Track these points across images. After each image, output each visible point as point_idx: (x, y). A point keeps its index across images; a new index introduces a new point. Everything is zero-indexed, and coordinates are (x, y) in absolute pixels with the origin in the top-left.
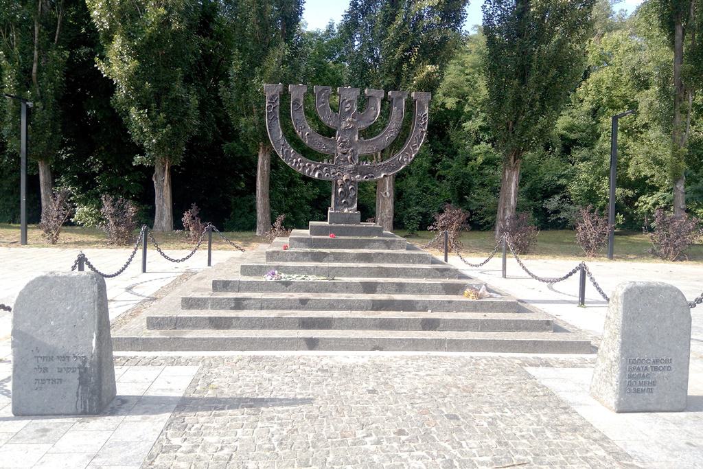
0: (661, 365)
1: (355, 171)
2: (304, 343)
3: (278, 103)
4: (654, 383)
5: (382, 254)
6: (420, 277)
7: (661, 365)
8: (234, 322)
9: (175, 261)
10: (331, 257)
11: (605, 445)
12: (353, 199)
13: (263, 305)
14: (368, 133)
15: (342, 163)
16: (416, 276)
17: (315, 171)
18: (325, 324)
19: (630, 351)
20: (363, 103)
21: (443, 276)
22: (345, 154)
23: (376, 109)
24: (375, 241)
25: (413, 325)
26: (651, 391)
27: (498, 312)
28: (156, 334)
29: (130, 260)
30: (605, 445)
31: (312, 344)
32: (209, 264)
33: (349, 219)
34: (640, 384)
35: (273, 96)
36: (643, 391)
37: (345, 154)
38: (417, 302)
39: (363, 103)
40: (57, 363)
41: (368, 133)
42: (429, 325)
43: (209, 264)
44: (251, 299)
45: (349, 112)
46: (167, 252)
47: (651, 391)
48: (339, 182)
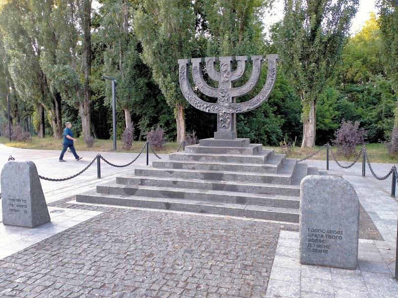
0: (334, 235)
1: (230, 107)
2: (164, 205)
3: (185, 70)
4: (328, 247)
5: (233, 157)
6: (252, 171)
7: (334, 235)
8: (186, 196)
9: (350, 166)
10: (203, 158)
11: (199, 289)
12: (229, 124)
13: (155, 183)
14: (236, 84)
15: (221, 103)
16: (249, 171)
17: (206, 108)
18: (181, 196)
19: (310, 223)
20: (234, 65)
21: (267, 172)
22: (224, 97)
23: (241, 67)
24: (233, 149)
25: (231, 200)
26: (326, 252)
27: (292, 195)
28: (99, 195)
29: (129, 164)
30: (199, 289)
31: (168, 206)
32: (147, 164)
33: (227, 137)
34: (318, 246)
35: (183, 66)
36: (320, 251)
37: (224, 97)
38: (239, 186)
39: (234, 65)
40: (17, 203)
41: (236, 84)
42: (241, 200)
43: (147, 164)
44: (148, 180)
45: (225, 71)
46: (339, 162)
47: (326, 252)
48: (221, 114)
